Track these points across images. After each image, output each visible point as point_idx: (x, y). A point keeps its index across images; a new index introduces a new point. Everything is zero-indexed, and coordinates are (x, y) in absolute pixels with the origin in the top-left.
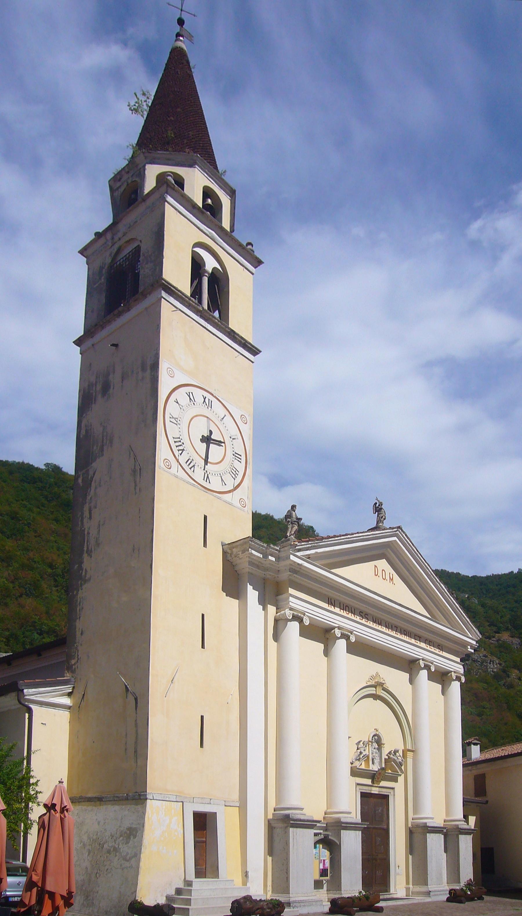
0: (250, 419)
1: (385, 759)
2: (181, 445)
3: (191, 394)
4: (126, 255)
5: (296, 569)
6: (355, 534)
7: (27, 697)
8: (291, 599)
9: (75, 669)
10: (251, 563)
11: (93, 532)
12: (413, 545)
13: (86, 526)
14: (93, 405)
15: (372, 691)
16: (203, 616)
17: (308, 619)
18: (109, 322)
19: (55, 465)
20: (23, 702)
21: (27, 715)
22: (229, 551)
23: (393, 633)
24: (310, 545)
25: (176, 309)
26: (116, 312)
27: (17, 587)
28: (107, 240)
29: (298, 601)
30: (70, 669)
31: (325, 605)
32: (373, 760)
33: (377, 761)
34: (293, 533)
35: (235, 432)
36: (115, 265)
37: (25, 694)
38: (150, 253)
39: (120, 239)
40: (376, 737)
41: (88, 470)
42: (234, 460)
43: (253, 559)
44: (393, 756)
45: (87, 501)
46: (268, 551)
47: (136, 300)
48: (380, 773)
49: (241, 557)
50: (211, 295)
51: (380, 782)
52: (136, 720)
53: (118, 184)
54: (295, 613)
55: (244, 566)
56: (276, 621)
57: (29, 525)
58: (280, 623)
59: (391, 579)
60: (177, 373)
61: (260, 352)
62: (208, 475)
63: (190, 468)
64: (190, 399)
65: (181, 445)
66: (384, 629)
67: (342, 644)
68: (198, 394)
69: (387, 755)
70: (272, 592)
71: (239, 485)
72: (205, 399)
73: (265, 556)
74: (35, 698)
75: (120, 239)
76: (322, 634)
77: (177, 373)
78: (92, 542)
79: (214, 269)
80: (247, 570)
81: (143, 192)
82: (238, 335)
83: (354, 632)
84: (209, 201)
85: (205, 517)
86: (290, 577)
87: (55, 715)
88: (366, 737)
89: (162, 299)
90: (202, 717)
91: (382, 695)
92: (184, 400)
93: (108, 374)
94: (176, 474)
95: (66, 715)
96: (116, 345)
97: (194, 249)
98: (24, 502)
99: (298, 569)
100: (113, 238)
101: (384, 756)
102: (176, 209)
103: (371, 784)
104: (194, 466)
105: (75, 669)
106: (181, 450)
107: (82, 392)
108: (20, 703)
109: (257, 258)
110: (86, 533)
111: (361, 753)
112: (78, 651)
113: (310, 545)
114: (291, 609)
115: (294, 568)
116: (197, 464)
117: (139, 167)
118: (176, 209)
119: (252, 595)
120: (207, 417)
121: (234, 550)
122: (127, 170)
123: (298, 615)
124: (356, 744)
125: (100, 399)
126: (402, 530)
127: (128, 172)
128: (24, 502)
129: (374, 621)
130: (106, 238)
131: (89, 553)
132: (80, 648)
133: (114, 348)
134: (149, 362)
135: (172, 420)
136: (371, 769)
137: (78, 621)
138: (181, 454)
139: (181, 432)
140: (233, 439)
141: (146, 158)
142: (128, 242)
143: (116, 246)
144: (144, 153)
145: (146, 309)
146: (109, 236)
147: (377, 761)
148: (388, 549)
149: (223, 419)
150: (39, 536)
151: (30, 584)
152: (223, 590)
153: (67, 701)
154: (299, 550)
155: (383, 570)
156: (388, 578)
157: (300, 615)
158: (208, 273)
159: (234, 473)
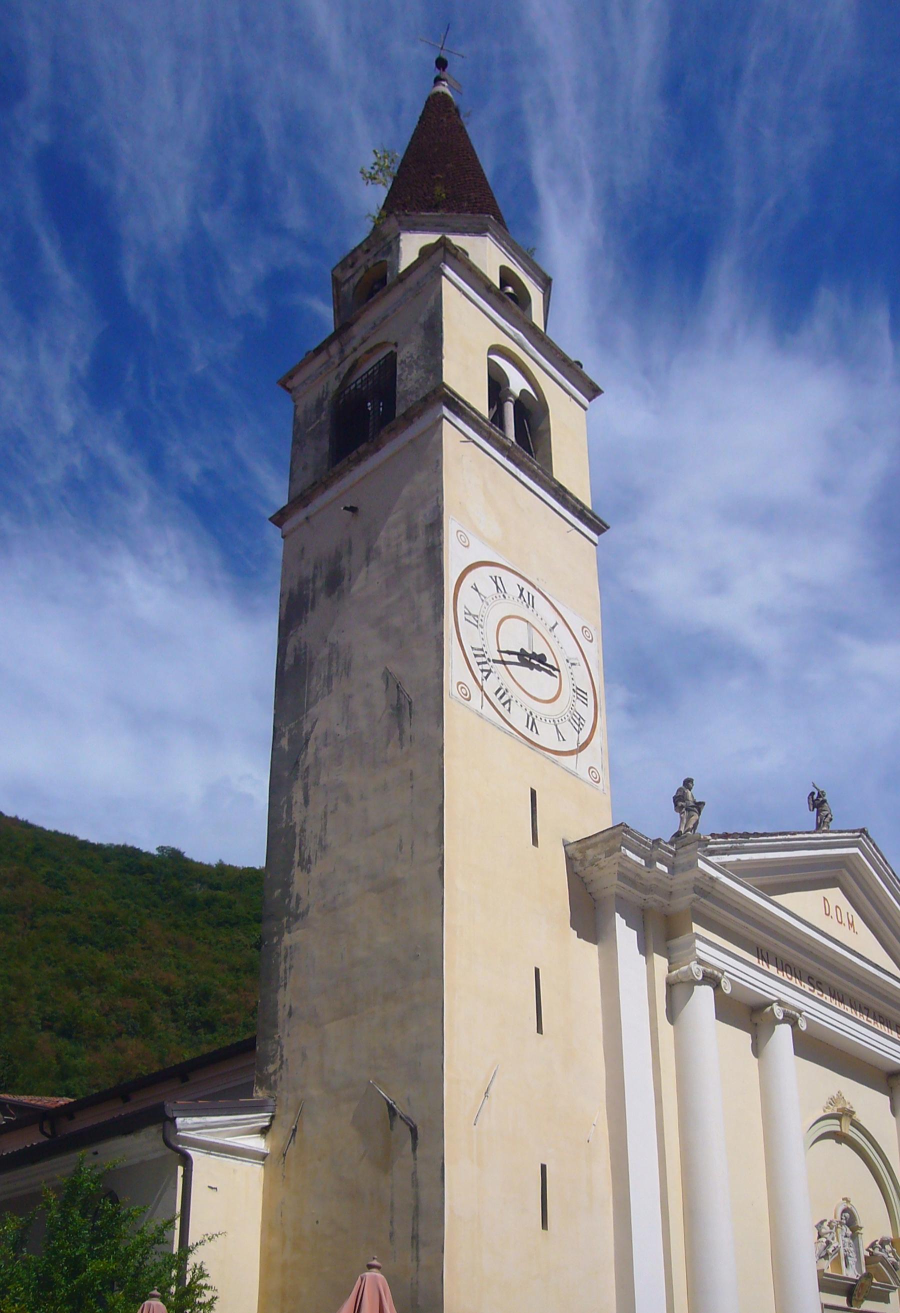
0: (597, 635)
1: (866, 1257)
2: (485, 663)
3: (498, 580)
4: (367, 372)
5: (706, 889)
6: (799, 833)
7: (181, 1134)
8: (698, 944)
9: (275, 1081)
10: (622, 876)
11: (313, 828)
12: (886, 863)
13: (297, 817)
14: (310, 614)
15: (832, 1126)
16: (537, 971)
17: (728, 982)
18: (340, 475)
19: (173, 849)
20: (174, 1144)
21: (180, 1170)
22: (578, 855)
23: (864, 1019)
24: (729, 845)
25: (466, 439)
26: (353, 455)
27: (113, 1022)
28: (330, 357)
29: (709, 949)
30: (264, 1082)
31: (753, 960)
32: (846, 1257)
33: (852, 1261)
34: (691, 826)
35: (574, 653)
36: (347, 392)
37: (178, 1127)
38: (415, 357)
39: (355, 350)
40: (847, 1215)
41: (301, 722)
42: (575, 699)
43: (626, 868)
44: (880, 1250)
45: (300, 774)
46: (655, 852)
47: (393, 429)
48: (862, 1285)
49: (602, 865)
50: (522, 432)
51: (863, 1301)
52: (414, 1173)
53: (350, 272)
54: (709, 970)
55: (607, 880)
56: (670, 985)
57: (133, 932)
58: (678, 991)
59: (851, 924)
60: (474, 541)
61: (608, 528)
62: (533, 720)
63: (504, 704)
64: (498, 587)
65: (485, 663)
66: (849, 1011)
67: (784, 1033)
68: (511, 583)
69: (867, 1250)
70: (661, 932)
71: (586, 744)
72: (522, 590)
73: (650, 863)
74: (196, 1137)
75: (355, 350)
76: (749, 1015)
77: (474, 541)
78: (312, 846)
79: (523, 392)
80: (613, 890)
81: (398, 269)
82: (571, 495)
83: (804, 1013)
84: (510, 289)
85: (533, 793)
86: (694, 904)
87: (234, 1171)
88: (832, 1213)
89: (444, 420)
90: (543, 1167)
91: (850, 1134)
92: (488, 588)
93: (338, 556)
94: (479, 709)
95: (255, 1172)
96: (353, 510)
97: (491, 357)
98: (127, 901)
99: (708, 889)
100: (342, 351)
101: (864, 1253)
102: (460, 289)
103: (845, 1305)
104: (509, 701)
105: (275, 1081)
106: (486, 671)
107: (287, 596)
108: (168, 1144)
109: (591, 383)
110: (297, 830)
111: (828, 1243)
112: (282, 1047)
113: (729, 845)
114: (701, 962)
115: (701, 886)
116: (514, 699)
117: (388, 239)
118: (460, 289)
119: (625, 936)
120: (527, 622)
121: (590, 853)
122: (365, 247)
123: (713, 974)
124: (816, 1226)
125: (323, 601)
126: (867, 836)
127: (368, 251)
128: (127, 901)
129: (833, 996)
130: (328, 353)
131: (306, 864)
132: (284, 1041)
133: (349, 513)
134: (422, 518)
135: (468, 617)
136: (845, 1275)
137: (281, 990)
138: (486, 678)
139: (485, 639)
140: (573, 664)
141: (400, 223)
142: (371, 352)
143: (347, 365)
144: (396, 216)
145: (411, 441)
146: (334, 349)
147: (852, 1261)
148: (844, 871)
149: (553, 628)
150: (149, 948)
151: (135, 1018)
152: (573, 925)
153: (258, 1143)
154: (712, 853)
155: (837, 907)
156: (845, 921)
157: (716, 972)
158: (514, 396)
159: (578, 723)
